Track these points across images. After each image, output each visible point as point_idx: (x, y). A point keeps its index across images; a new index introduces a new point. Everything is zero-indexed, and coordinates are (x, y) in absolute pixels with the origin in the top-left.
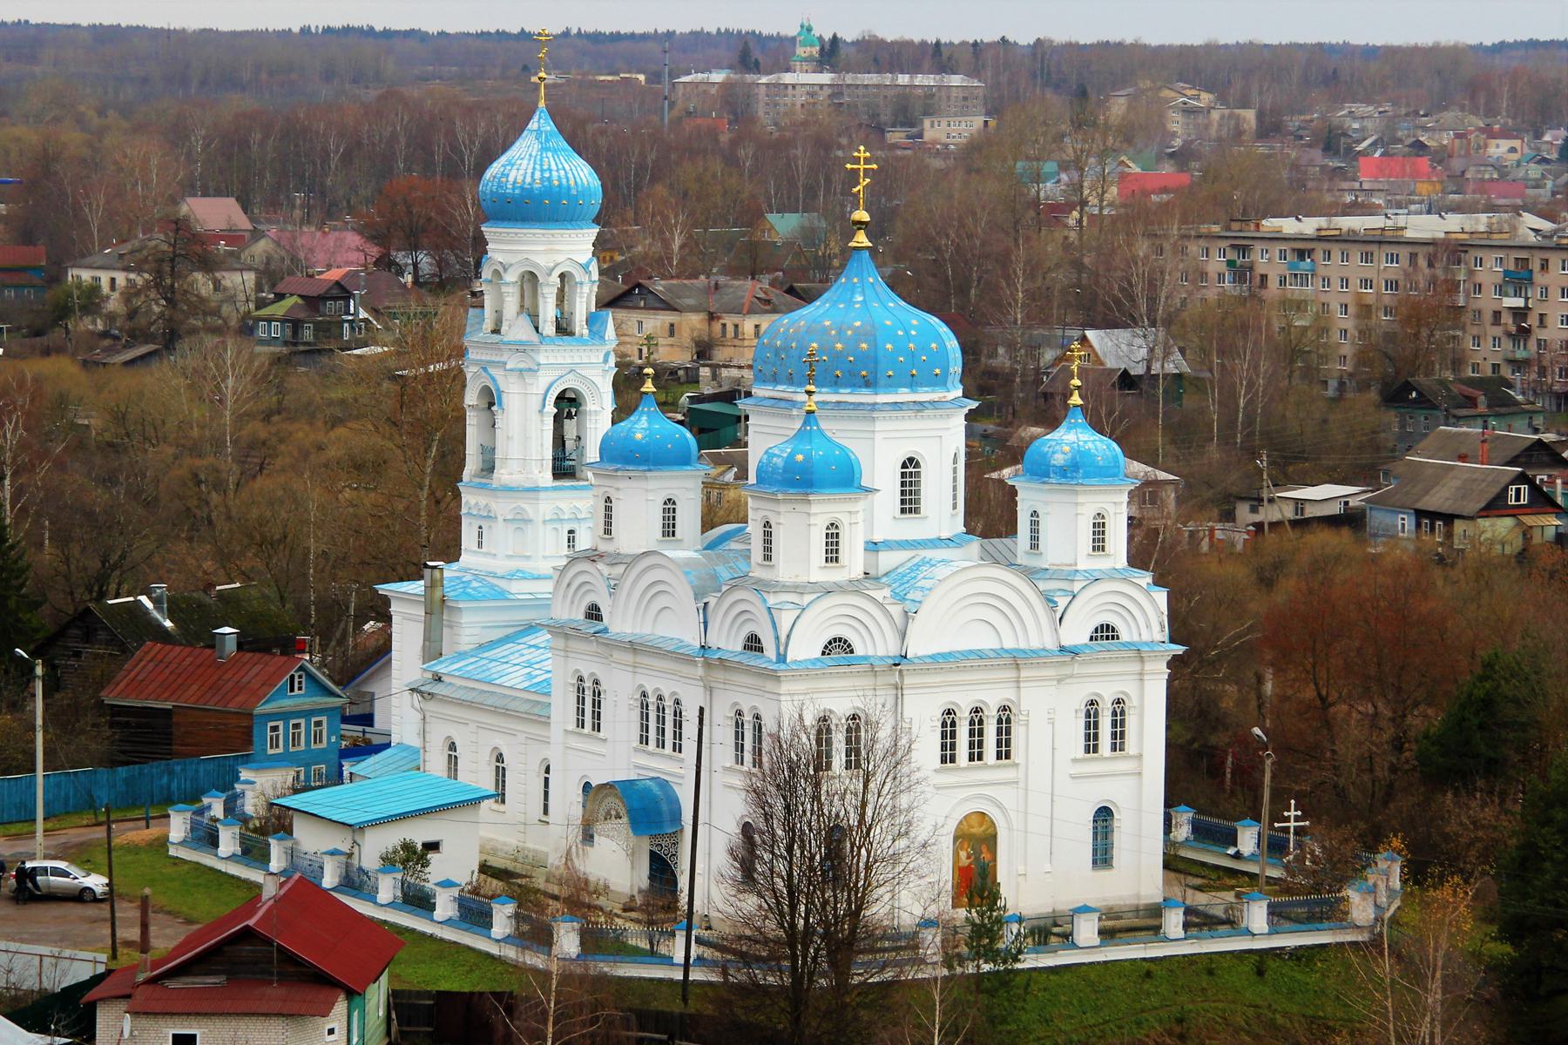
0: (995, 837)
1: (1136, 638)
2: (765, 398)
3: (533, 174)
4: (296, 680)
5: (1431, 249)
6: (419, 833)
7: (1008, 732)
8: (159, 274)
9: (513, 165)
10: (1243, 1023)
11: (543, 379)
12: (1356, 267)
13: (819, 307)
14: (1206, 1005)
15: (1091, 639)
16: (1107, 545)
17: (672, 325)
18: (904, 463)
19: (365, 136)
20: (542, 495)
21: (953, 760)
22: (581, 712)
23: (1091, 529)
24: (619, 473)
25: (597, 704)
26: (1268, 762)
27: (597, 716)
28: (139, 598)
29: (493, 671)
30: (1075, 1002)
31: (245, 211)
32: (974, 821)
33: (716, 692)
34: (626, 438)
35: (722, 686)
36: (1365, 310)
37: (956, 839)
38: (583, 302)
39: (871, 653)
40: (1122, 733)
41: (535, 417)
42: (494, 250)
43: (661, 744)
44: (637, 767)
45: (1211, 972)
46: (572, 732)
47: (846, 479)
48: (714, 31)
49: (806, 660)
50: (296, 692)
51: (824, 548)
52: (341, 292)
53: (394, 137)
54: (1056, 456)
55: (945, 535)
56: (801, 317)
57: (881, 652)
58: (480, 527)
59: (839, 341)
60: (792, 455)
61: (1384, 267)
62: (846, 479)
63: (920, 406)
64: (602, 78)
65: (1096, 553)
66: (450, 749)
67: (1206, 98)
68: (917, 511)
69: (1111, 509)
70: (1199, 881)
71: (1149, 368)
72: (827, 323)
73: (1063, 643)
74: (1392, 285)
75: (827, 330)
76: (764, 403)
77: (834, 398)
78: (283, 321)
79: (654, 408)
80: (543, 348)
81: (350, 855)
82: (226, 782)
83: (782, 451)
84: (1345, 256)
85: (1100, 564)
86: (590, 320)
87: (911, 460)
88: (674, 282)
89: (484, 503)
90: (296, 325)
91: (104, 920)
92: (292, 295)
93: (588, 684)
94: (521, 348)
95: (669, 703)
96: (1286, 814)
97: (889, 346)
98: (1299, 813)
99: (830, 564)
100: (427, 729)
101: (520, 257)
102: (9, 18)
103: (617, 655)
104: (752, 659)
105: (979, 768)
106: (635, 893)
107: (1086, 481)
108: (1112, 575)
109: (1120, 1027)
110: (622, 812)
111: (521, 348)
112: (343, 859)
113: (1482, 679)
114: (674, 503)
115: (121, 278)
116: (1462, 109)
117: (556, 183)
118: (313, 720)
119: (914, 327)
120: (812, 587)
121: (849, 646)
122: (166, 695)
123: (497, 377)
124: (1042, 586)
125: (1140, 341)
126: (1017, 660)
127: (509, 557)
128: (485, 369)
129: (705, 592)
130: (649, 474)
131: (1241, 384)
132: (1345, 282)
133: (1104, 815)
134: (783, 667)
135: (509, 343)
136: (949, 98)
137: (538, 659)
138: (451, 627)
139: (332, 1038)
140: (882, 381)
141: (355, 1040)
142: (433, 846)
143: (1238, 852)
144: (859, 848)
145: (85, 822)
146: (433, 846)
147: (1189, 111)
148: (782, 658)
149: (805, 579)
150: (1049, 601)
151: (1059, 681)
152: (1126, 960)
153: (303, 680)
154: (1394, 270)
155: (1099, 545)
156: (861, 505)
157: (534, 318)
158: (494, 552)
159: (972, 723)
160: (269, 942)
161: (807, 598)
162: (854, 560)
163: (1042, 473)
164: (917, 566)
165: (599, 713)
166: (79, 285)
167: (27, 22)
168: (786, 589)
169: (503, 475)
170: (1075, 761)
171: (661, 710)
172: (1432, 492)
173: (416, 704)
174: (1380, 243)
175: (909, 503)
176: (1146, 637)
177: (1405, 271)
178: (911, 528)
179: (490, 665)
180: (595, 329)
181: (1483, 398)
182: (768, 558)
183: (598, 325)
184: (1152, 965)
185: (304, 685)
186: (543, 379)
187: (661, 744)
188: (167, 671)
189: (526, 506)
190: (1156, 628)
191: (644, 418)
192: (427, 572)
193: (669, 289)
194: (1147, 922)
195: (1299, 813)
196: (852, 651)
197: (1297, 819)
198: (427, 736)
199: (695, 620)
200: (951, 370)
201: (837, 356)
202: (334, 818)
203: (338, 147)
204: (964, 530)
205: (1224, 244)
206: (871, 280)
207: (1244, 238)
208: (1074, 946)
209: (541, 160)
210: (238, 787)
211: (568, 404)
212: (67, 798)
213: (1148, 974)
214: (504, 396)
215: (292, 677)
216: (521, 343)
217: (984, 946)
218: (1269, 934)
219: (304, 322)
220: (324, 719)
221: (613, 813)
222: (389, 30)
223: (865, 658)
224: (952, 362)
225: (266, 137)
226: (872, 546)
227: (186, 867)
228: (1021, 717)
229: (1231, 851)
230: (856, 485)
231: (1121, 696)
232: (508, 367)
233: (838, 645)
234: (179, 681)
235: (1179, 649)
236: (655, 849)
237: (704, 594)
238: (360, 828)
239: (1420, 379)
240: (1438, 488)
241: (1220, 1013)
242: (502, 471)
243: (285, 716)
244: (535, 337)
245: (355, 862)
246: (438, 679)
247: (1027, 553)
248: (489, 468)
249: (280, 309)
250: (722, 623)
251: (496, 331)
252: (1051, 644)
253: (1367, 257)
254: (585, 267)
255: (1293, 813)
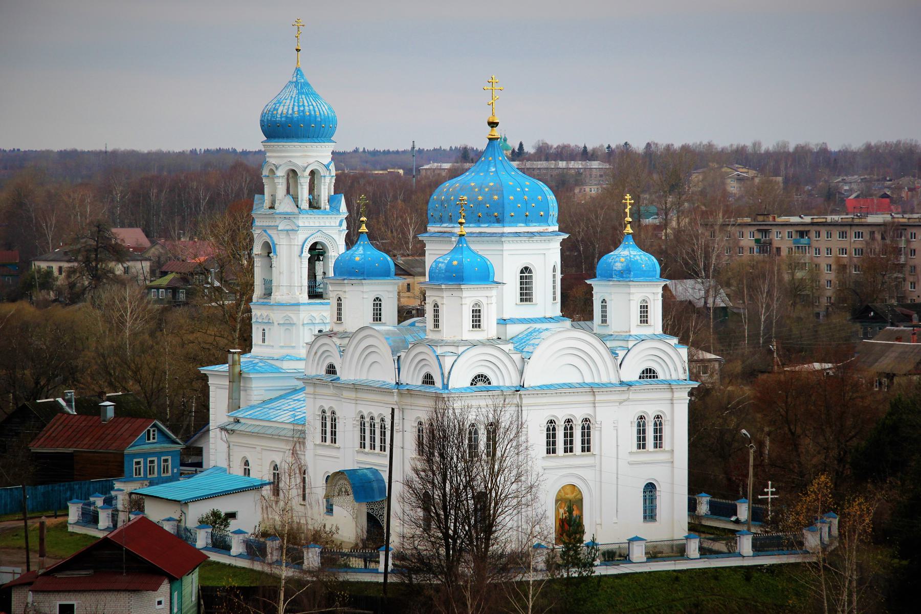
0: (581, 500)
1: (668, 378)
2: (435, 233)
3: (293, 108)
4: (151, 433)
5: (883, 227)
6: (223, 506)
7: (589, 435)
8: (87, 261)
9: (281, 103)
10: (737, 608)
11: (301, 237)
12: (836, 242)
13: (467, 176)
14: (714, 597)
15: (640, 377)
16: (649, 319)
17: (409, 285)
18: (522, 270)
19: (222, 190)
20: (302, 308)
21: (554, 452)
22: (324, 432)
23: (639, 310)
24: (346, 282)
25: (334, 426)
26: (752, 451)
27: (334, 433)
28: (57, 399)
29: (272, 414)
30: (630, 595)
31: (147, 236)
32: (568, 490)
33: (406, 411)
34: (349, 260)
35: (409, 407)
36: (842, 268)
37: (557, 501)
38: (326, 188)
39: (501, 384)
40: (661, 437)
41: (297, 259)
42: (270, 157)
43: (373, 447)
44: (358, 463)
45: (716, 578)
46: (319, 445)
47: (485, 276)
48: (448, 149)
49: (461, 388)
50: (152, 441)
51: (471, 319)
52: (204, 271)
53: (241, 189)
54: (617, 264)
55: (548, 316)
56: (457, 182)
57: (508, 384)
58: (264, 330)
59: (480, 195)
60: (450, 262)
61: (853, 242)
62: (485, 276)
63: (532, 234)
64: (376, 172)
65: (643, 324)
66: (245, 465)
67: (752, 173)
68: (530, 300)
69: (651, 297)
70: (712, 536)
71: (706, 303)
72: (473, 184)
73: (622, 380)
74: (859, 251)
75: (473, 188)
76: (434, 235)
77: (478, 230)
78: (166, 289)
79: (367, 242)
80: (301, 216)
81: (180, 521)
82: (106, 489)
83: (444, 259)
84: (829, 235)
85: (645, 331)
86: (330, 200)
87: (526, 268)
88: (410, 258)
89: (266, 314)
90: (174, 290)
91: (24, 563)
92: (172, 272)
93: (328, 414)
94: (287, 216)
95: (377, 421)
96: (766, 490)
97: (511, 197)
98: (774, 490)
99: (475, 329)
100: (231, 454)
101: (286, 160)
102: (8, 147)
103: (346, 394)
104: (429, 389)
105: (587, 456)
106: (359, 541)
107: (635, 279)
108: (654, 337)
109: (659, 610)
110: (350, 492)
111: (287, 216)
112: (175, 523)
113: (890, 414)
114: (380, 300)
115: (65, 265)
116: (914, 176)
117: (308, 113)
118: (163, 458)
119: (527, 186)
120: (464, 342)
121: (488, 380)
122: (70, 444)
123: (272, 235)
124: (609, 344)
125: (698, 286)
126: (593, 389)
127: (282, 347)
128: (265, 231)
129: (398, 350)
130: (364, 282)
131: (762, 307)
132: (829, 250)
133: (650, 488)
134: (446, 391)
135: (280, 214)
136: (591, 175)
137: (299, 407)
138: (246, 390)
139: (160, 606)
140: (507, 218)
141: (175, 610)
142: (232, 515)
143: (738, 519)
144: (491, 489)
145: (17, 518)
146: (232, 515)
147: (740, 179)
148: (446, 386)
149: (460, 338)
150: (614, 353)
151: (620, 403)
152: (663, 571)
153: (156, 433)
154: (859, 243)
155: (644, 319)
156: (494, 292)
157: (295, 199)
158: (272, 344)
159: (566, 429)
160: (120, 548)
161: (461, 349)
162: (490, 328)
163: (609, 275)
164: (531, 333)
165: (335, 432)
166: (39, 271)
167: (18, 150)
168: (448, 344)
169: (277, 296)
170: (631, 453)
171: (372, 426)
172: (880, 360)
173: (224, 436)
174: (851, 225)
175: (526, 295)
176: (674, 377)
177: (866, 242)
178: (526, 311)
179: (269, 412)
180: (333, 205)
181: (916, 315)
182: (437, 326)
183: (336, 202)
184: (679, 574)
185: (156, 436)
186: (301, 237)
187: (373, 447)
188: (71, 430)
189: (290, 315)
190: (681, 371)
191: (361, 248)
192: (230, 356)
193: (406, 262)
194: (680, 552)
195: (774, 490)
196: (490, 383)
197: (773, 493)
198: (231, 457)
199: (392, 366)
200: (551, 213)
201: (479, 204)
202: (169, 498)
203: (205, 196)
204: (561, 314)
205: (753, 229)
206: (500, 158)
207: (766, 225)
208: (630, 562)
209: (298, 100)
210: (113, 493)
211: (317, 252)
212: (6, 505)
213: (677, 579)
214: (277, 247)
215: (149, 431)
216: (287, 214)
217: (571, 556)
218: (753, 556)
219: (179, 288)
220: (169, 458)
221: (343, 490)
222: (246, 151)
223: (498, 387)
224: (551, 209)
225: (161, 191)
226: (502, 321)
227: (78, 537)
228: (597, 425)
229: (733, 518)
230: (491, 279)
231: (659, 414)
232: (279, 228)
233: (480, 378)
234: (78, 436)
235: (695, 385)
236: (370, 511)
237: (398, 351)
238: (186, 503)
239: (878, 304)
240: (884, 358)
241: (722, 602)
242: (277, 294)
243: (145, 455)
244: (296, 210)
245: (183, 524)
246: (237, 421)
247: (599, 325)
248: (268, 293)
249: (165, 281)
250: (409, 367)
251: (272, 207)
252: (614, 380)
253: (843, 235)
254: (327, 167)
255: (770, 490)
